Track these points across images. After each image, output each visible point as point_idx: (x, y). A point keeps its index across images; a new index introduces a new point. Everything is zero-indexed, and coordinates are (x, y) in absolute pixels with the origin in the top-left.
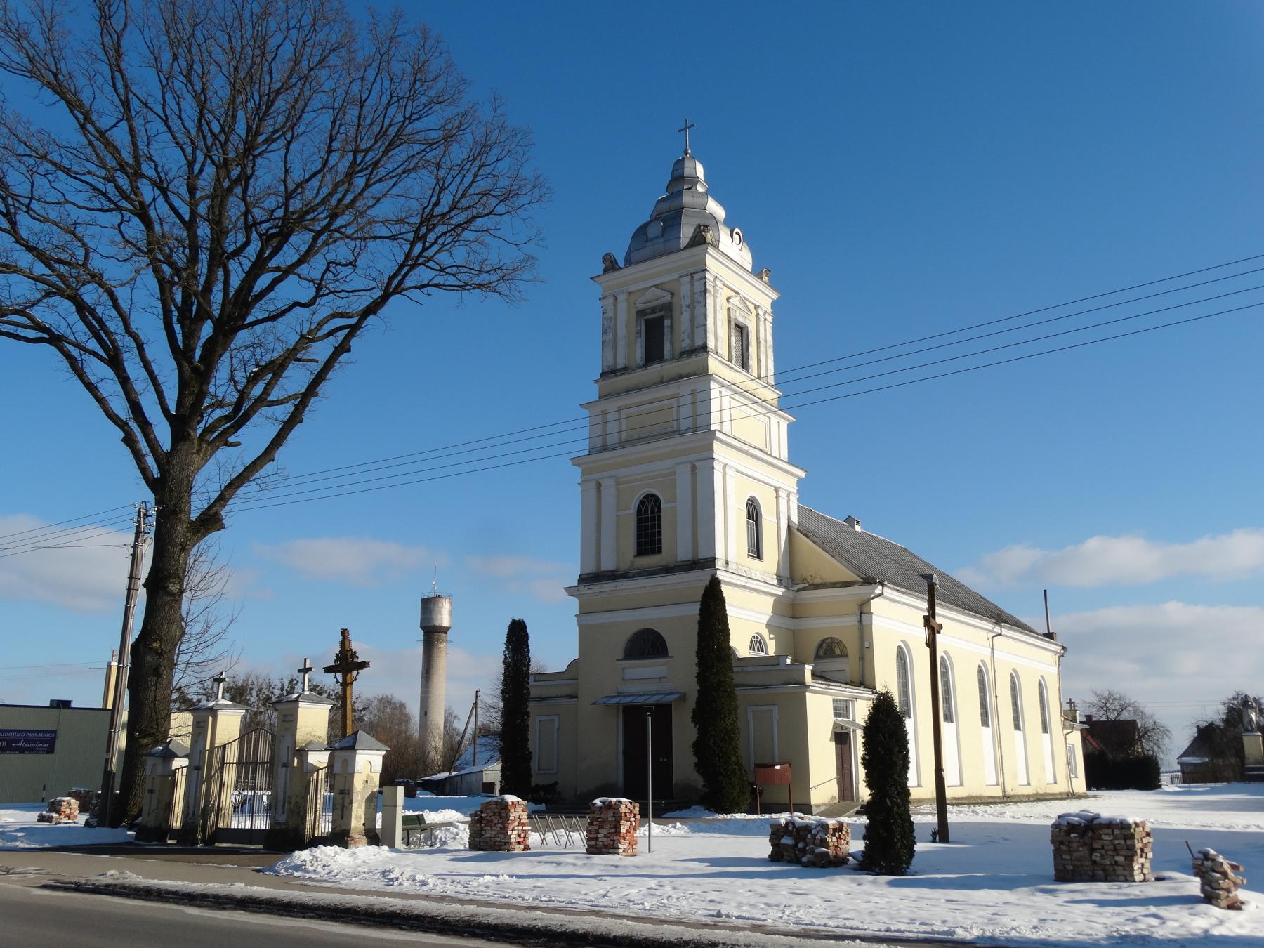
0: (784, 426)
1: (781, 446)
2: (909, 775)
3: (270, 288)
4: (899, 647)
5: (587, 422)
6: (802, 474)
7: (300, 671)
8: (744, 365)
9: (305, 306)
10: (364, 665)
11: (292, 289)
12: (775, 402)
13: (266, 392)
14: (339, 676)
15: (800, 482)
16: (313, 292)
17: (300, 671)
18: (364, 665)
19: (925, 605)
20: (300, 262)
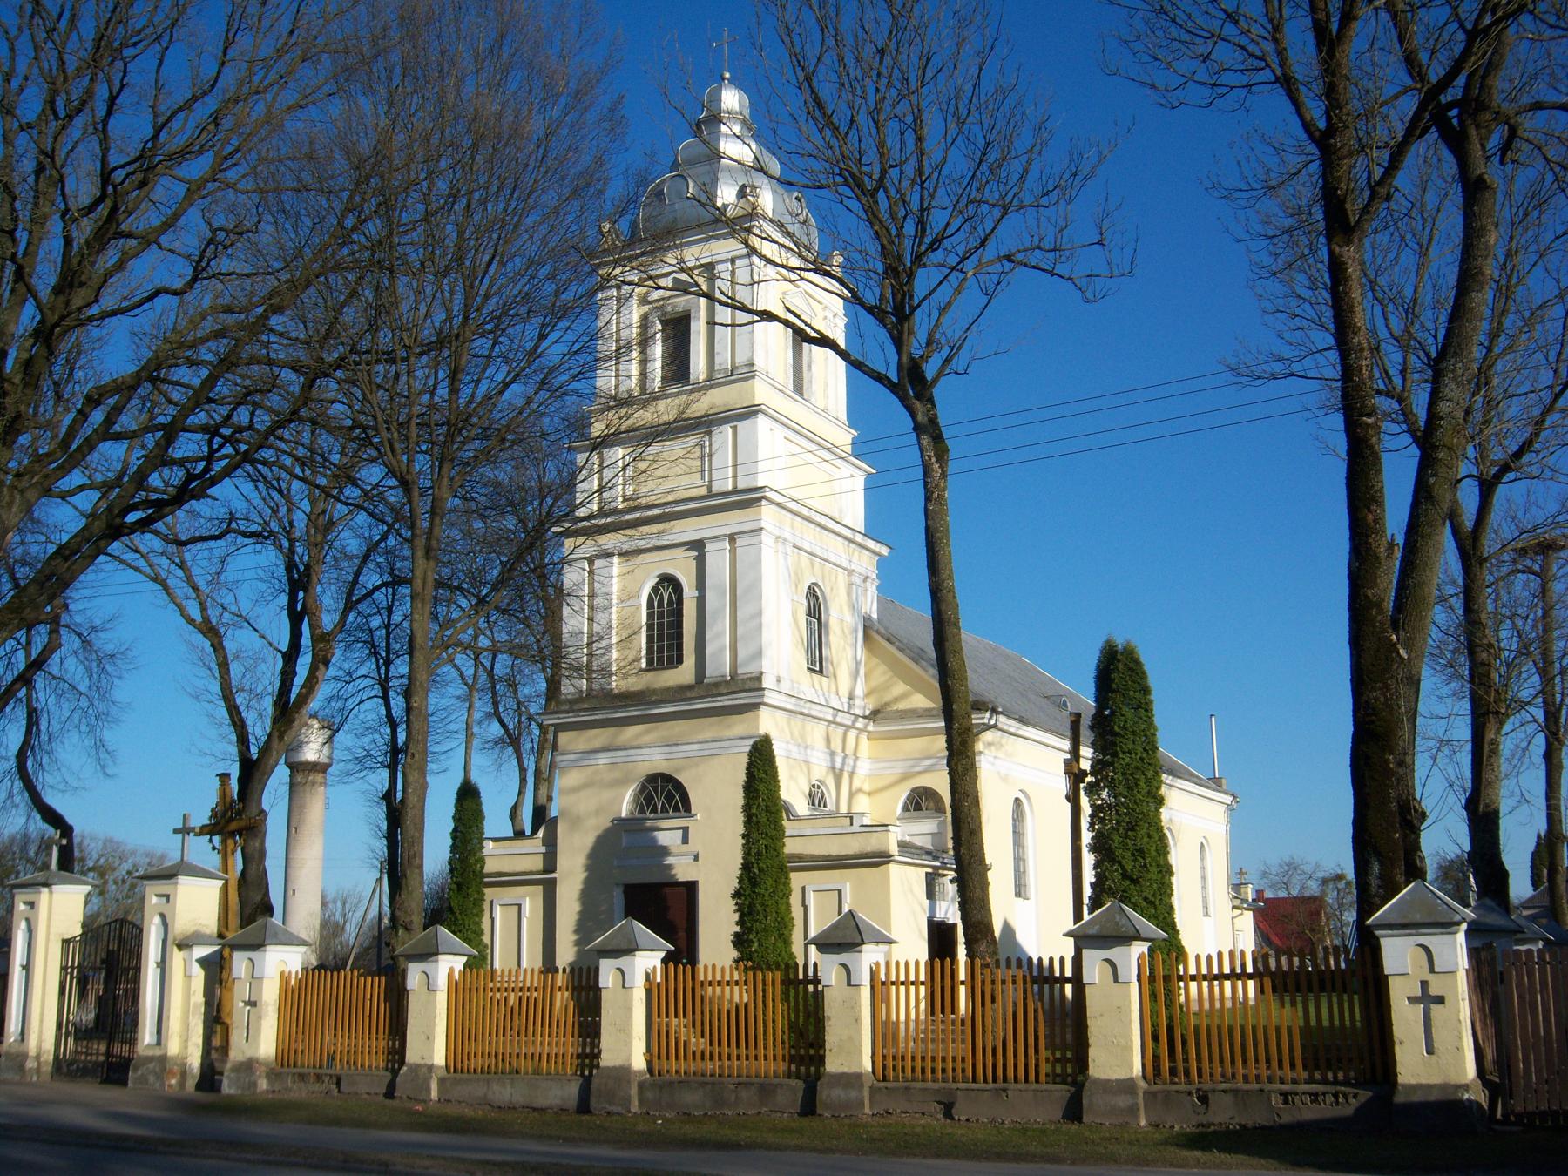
0: (860, 482)
1: (854, 510)
2: (577, 907)
3: (120, 266)
4: (1017, 799)
5: (761, 467)
6: (884, 551)
7: (176, 831)
8: (799, 387)
9: (175, 293)
10: (1068, 935)
11: (154, 269)
12: (849, 449)
13: (109, 421)
14: (217, 839)
15: (882, 563)
16: (189, 272)
17: (176, 831)
18: (1068, 935)
19: (1066, 745)
20: (168, 225)
